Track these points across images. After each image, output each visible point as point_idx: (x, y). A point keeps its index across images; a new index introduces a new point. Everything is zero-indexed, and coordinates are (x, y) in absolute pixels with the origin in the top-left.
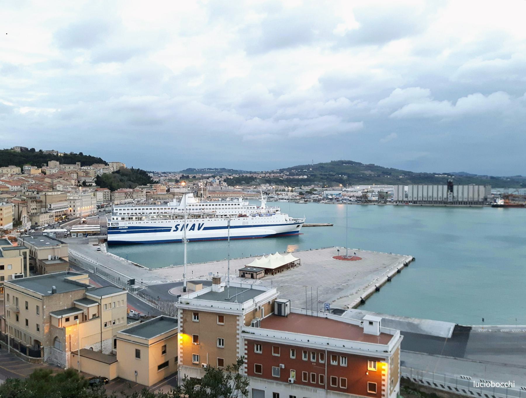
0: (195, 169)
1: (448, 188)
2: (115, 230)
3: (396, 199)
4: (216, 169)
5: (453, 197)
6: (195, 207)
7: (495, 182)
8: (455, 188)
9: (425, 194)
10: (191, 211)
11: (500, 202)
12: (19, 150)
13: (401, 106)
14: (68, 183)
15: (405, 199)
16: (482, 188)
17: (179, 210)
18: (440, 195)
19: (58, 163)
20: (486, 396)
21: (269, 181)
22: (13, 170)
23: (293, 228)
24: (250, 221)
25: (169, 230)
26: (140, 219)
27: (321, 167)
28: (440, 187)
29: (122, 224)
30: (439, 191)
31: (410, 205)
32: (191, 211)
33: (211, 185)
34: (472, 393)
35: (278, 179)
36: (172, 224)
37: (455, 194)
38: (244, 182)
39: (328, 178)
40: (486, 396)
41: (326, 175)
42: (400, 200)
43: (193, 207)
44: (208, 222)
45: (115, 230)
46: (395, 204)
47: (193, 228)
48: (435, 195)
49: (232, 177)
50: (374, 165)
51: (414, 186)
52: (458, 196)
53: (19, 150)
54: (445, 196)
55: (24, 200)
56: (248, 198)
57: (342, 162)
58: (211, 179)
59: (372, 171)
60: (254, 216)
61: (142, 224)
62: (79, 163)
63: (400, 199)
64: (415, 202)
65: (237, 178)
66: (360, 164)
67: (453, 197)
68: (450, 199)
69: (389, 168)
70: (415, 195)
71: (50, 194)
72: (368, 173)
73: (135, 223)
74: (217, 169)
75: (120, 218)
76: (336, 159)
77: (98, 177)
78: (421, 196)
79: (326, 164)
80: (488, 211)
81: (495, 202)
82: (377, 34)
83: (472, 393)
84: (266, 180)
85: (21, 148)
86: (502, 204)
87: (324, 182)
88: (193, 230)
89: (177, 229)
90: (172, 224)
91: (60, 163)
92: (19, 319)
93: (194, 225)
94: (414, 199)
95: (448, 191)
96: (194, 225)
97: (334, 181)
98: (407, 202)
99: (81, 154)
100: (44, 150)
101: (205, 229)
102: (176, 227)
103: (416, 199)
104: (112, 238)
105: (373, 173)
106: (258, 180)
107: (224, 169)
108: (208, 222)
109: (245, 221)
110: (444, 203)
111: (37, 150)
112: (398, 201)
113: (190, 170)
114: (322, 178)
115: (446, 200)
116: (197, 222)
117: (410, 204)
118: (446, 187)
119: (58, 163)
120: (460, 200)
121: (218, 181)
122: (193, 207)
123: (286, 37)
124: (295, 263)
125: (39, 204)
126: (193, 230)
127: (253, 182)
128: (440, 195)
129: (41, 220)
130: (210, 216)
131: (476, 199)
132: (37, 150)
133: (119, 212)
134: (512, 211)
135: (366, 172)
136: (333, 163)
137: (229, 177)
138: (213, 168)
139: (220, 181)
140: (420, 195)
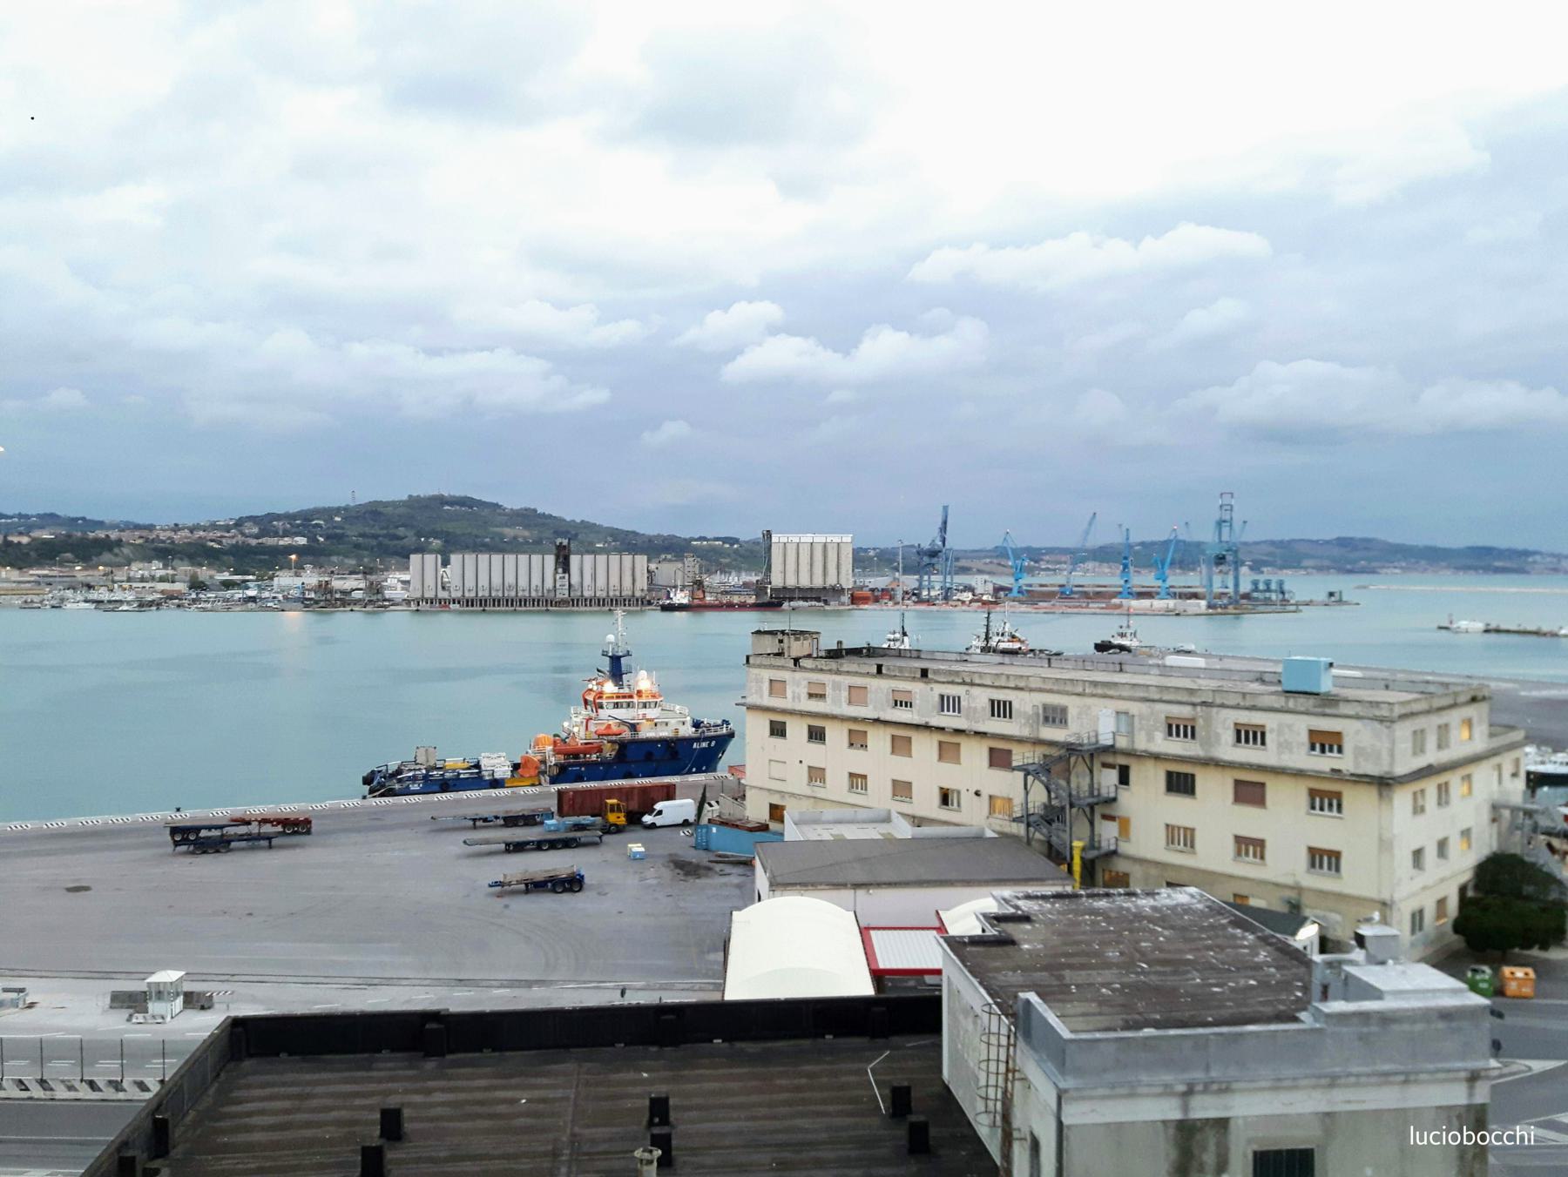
3: (418, 595)
4: (20, 516)
7: (671, 548)
11: (680, 598)
13: (736, 352)
15: (442, 594)
16: (641, 560)
21: (165, 553)
28: (536, 558)
31: (455, 611)
34: (92, 1085)
35: (204, 546)
37: (575, 580)
38: (69, 555)
39: (380, 545)
41: (375, 537)
49: (25, 540)
54: (549, 584)
57: (441, 500)
59: (526, 527)
63: (429, 594)
65: (45, 542)
66: (497, 506)
68: (562, 593)
69: (578, 520)
72: (520, 532)
74: (27, 517)
76: (426, 490)
78: (486, 585)
79: (393, 504)
81: (669, 598)
82: (703, 116)
83: (92, 1085)
84: (155, 549)
86: (685, 601)
87: (359, 558)
98: (444, 604)
103: (473, 594)
105: (526, 533)
106: (126, 551)
107: (52, 516)
110: (546, 603)
114: (357, 546)
118: (550, 560)
120: (587, 594)
123: (467, 93)
124: (436, 788)
127: (106, 556)
131: (627, 593)
134: (711, 617)
135: (507, 531)
136: (416, 504)
137: (15, 539)
138: (10, 513)
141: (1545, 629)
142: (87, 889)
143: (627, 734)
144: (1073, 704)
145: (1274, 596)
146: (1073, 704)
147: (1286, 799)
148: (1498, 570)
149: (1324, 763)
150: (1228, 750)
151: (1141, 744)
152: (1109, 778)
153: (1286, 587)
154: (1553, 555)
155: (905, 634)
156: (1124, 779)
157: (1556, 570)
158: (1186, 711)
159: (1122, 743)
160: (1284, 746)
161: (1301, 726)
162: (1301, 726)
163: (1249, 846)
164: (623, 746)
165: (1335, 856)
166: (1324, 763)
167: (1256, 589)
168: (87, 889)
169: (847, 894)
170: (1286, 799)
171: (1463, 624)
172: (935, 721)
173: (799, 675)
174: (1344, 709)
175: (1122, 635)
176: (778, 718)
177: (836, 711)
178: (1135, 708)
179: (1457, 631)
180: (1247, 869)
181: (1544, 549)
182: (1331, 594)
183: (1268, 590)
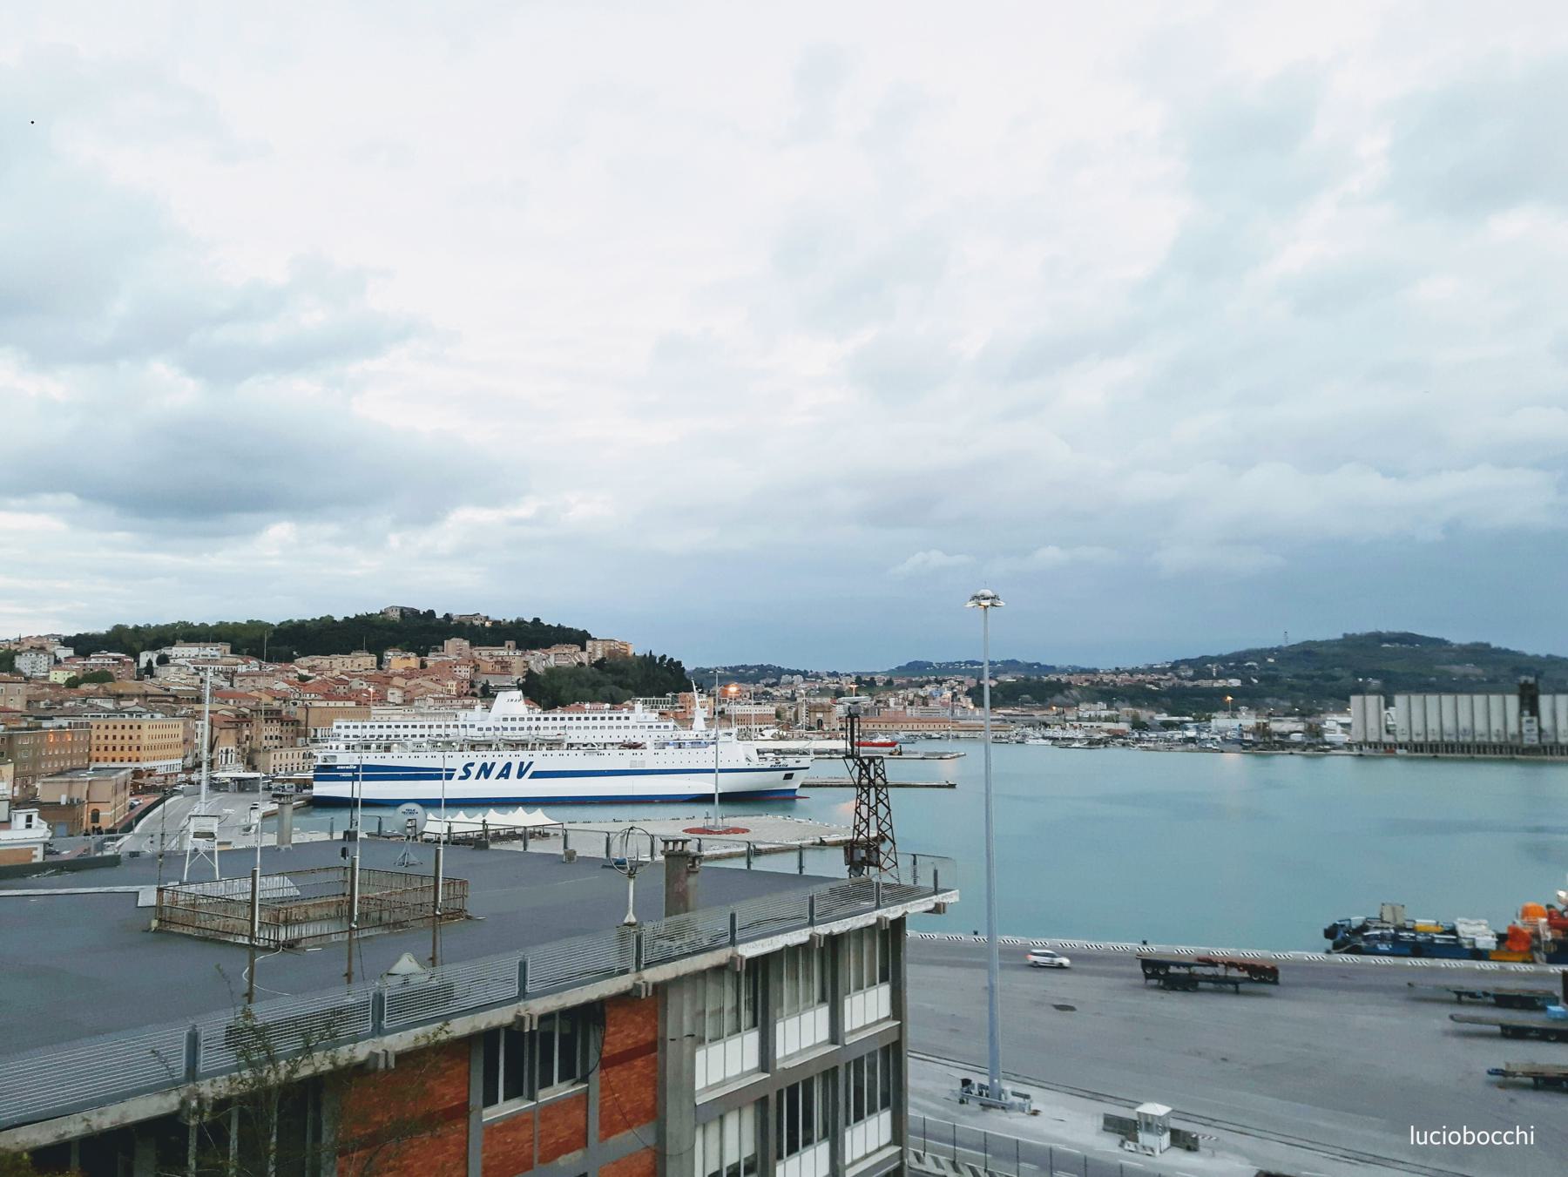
0: (930, 664)
1: (1522, 706)
2: (328, 772)
3: (1360, 738)
5: (1540, 730)
6: (517, 724)
8: (1544, 702)
9: (1448, 724)
10: (542, 732)
12: (396, 615)
14: (439, 688)
15: (1387, 739)
17: (480, 729)
18: (1496, 725)
19: (467, 643)
20: (972, 1169)
22: (357, 662)
23: (774, 781)
24: (647, 759)
25: (449, 777)
26: (388, 749)
27: (1307, 653)
28: (1495, 700)
29: (345, 759)
30: (1496, 714)
32: (542, 732)
33: (926, 704)
35: (1144, 688)
36: (457, 761)
37: (1546, 723)
40: (972, 1169)
42: (1370, 739)
43: (513, 724)
44: (543, 760)
45: (328, 772)
46: (1356, 751)
47: (505, 773)
48: (1480, 726)
50: (1488, 645)
51: (1429, 697)
52: (1555, 729)
53: (396, 615)
55: (245, 716)
56: (962, 734)
57: (1378, 638)
58: (929, 689)
59: (1477, 664)
60: (664, 745)
61: (389, 760)
62: (512, 643)
63: (1372, 738)
64: (1419, 747)
65: (1010, 685)
67: (1540, 730)
68: (1531, 739)
70: (1417, 726)
71: (316, 704)
73: (373, 758)
75: (342, 746)
77: (530, 674)
78: (1437, 728)
85: (402, 609)
88: (507, 777)
89: (468, 773)
90: (457, 761)
91: (472, 645)
93: (508, 766)
94: (1415, 739)
95: (1521, 714)
96: (508, 766)
97: (1332, 695)
99: (537, 620)
100: (456, 613)
101: (535, 775)
102: (465, 769)
103: (1421, 739)
104: (321, 789)
106: (1074, 692)
107: (1014, 662)
108: (543, 760)
109: (638, 758)
110: (1508, 751)
111: (439, 615)
112: (1366, 743)
113: (916, 667)
114: (1292, 687)
115: (1517, 741)
116: (517, 758)
117: (1398, 751)
118: (1513, 701)
119: (467, 643)
121: (948, 694)
122: (513, 724)
125: (290, 728)
126: (507, 777)
127: (1058, 698)
128: (1496, 725)
129: (272, 762)
130: (553, 744)
132: (439, 615)
133: (343, 732)
135: (1456, 669)
136: (1350, 642)
139: (954, 695)
140: (1433, 724)
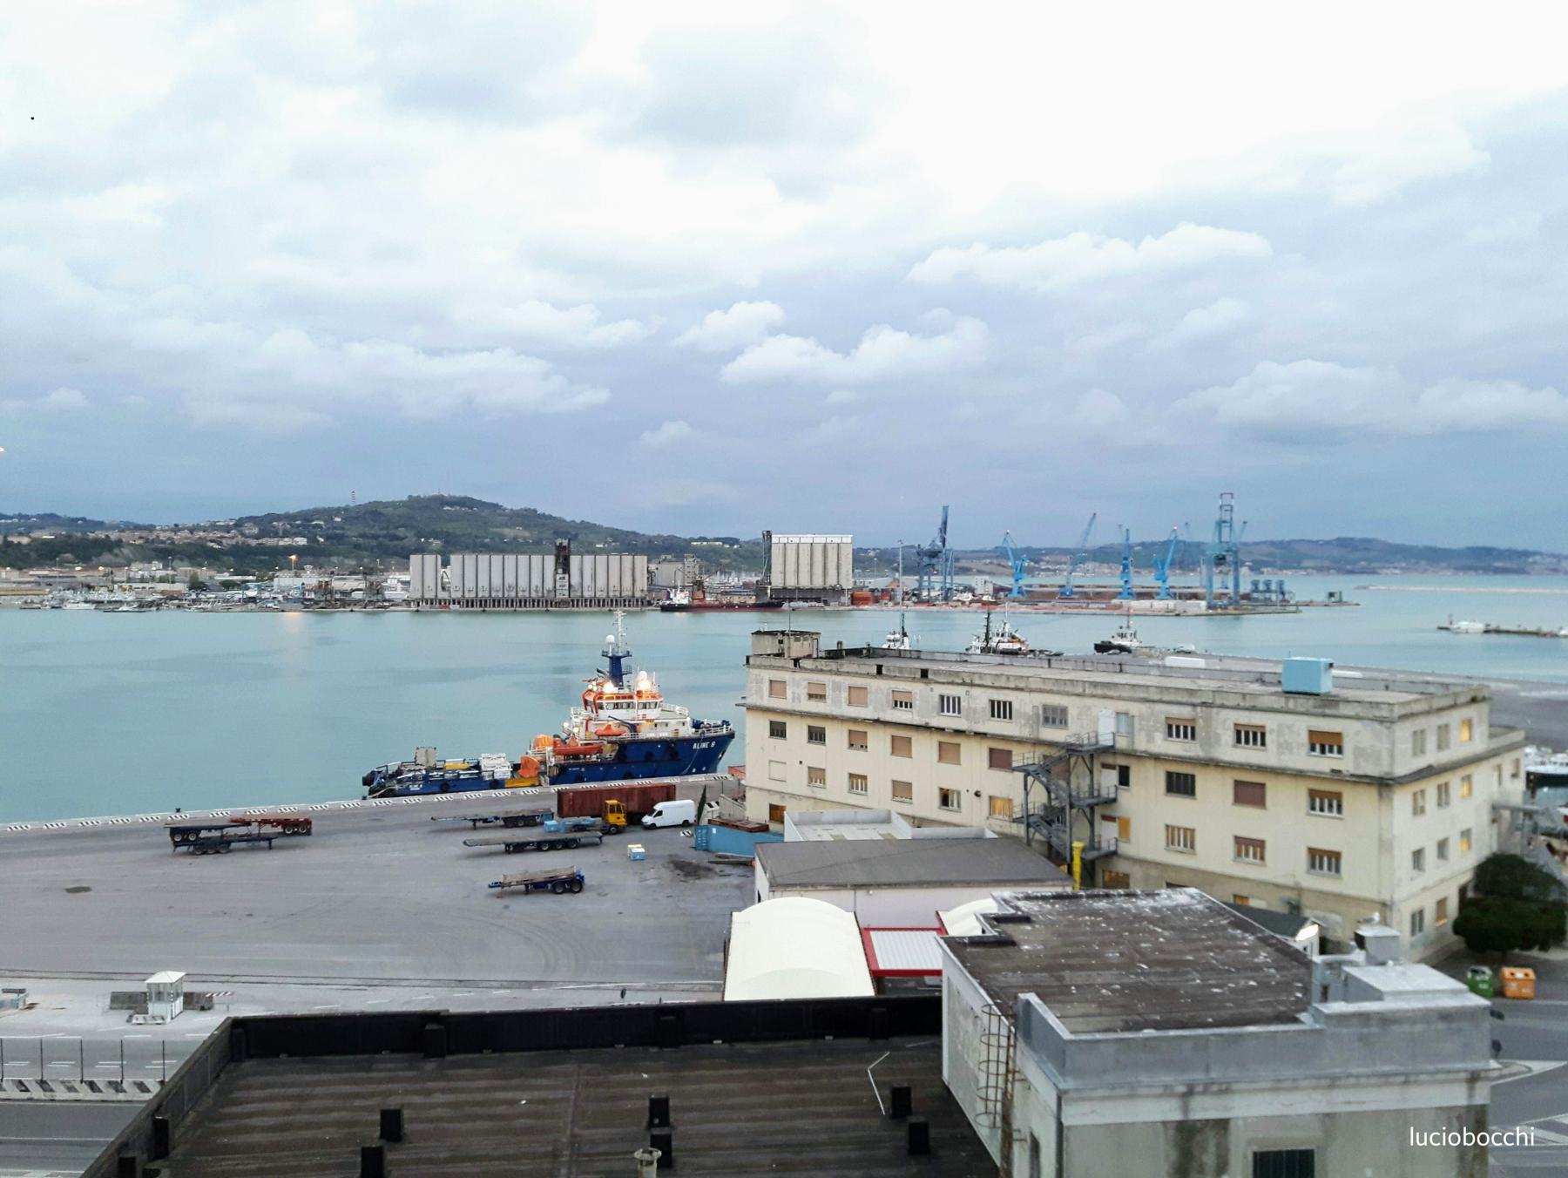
3: (418, 595)
4: (20, 516)
7: (671, 548)
11: (680, 598)
13: (736, 352)
15: (442, 595)
16: (641, 560)
21: (165, 553)
28: (536, 559)
31: (455, 612)
34: (92, 1086)
35: (204, 547)
37: (575, 580)
38: (69, 556)
39: (380, 545)
41: (375, 537)
49: (25, 540)
54: (549, 584)
57: (441, 501)
59: (526, 527)
63: (429, 595)
65: (45, 543)
66: (497, 506)
68: (562, 594)
69: (578, 521)
72: (520, 532)
74: (27, 517)
76: (426, 490)
78: (486, 586)
79: (393, 504)
80: (656, 618)
81: (669, 598)
83: (92, 1086)
84: (155, 550)
86: (685, 602)
87: (359, 559)
92: (71, 895)
98: (444, 604)
103: (473, 595)
105: (526, 534)
106: (126, 551)
107: (52, 516)
110: (546, 604)
114: (357, 547)
118: (550, 560)
120: (587, 594)
127: (106, 557)
131: (627, 593)
134: (711, 617)
135: (507, 531)
136: (416, 504)
137: (15, 540)
138: (10, 513)
141: (1545, 629)
142: (87, 889)
143: (627, 735)
144: (1073, 705)
145: (1274, 597)
146: (1073, 705)
147: (1286, 800)
148: (1498, 571)
149: (1324, 763)
150: (1228, 751)
151: (1141, 745)
152: (1109, 779)
153: (1286, 588)
154: (1553, 556)
155: (905, 635)
156: (1124, 779)
157: (1556, 571)
158: (1186, 712)
159: (1122, 744)
160: (1284, 747)
161: (1301, 726)
162: (1301, 726)
163: (1249, 847)
164: (623, 747)
165: (1335, 857)
166: (1324, 763)
167: (1256, 590)
168: (87, 889)
169: (847, 895)
170: (1286, 800)
171: (1463, 624)
172: (935, 722)
173: (799, 676)
174: (1344, 709)
175: (1122, 636)
176: (778, 718)
177: (836, 712)
178: (1135, 708)
179: (1457, 632)
180: (1247, 870)
181: (1544, 549)
182: (1331, 595)
183: (1268, 590)
